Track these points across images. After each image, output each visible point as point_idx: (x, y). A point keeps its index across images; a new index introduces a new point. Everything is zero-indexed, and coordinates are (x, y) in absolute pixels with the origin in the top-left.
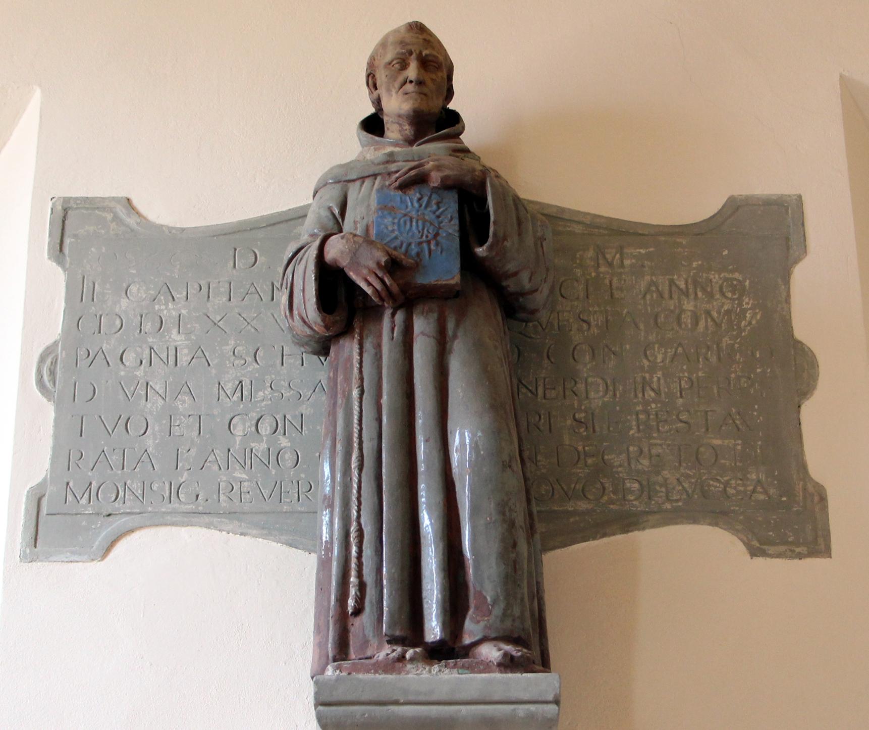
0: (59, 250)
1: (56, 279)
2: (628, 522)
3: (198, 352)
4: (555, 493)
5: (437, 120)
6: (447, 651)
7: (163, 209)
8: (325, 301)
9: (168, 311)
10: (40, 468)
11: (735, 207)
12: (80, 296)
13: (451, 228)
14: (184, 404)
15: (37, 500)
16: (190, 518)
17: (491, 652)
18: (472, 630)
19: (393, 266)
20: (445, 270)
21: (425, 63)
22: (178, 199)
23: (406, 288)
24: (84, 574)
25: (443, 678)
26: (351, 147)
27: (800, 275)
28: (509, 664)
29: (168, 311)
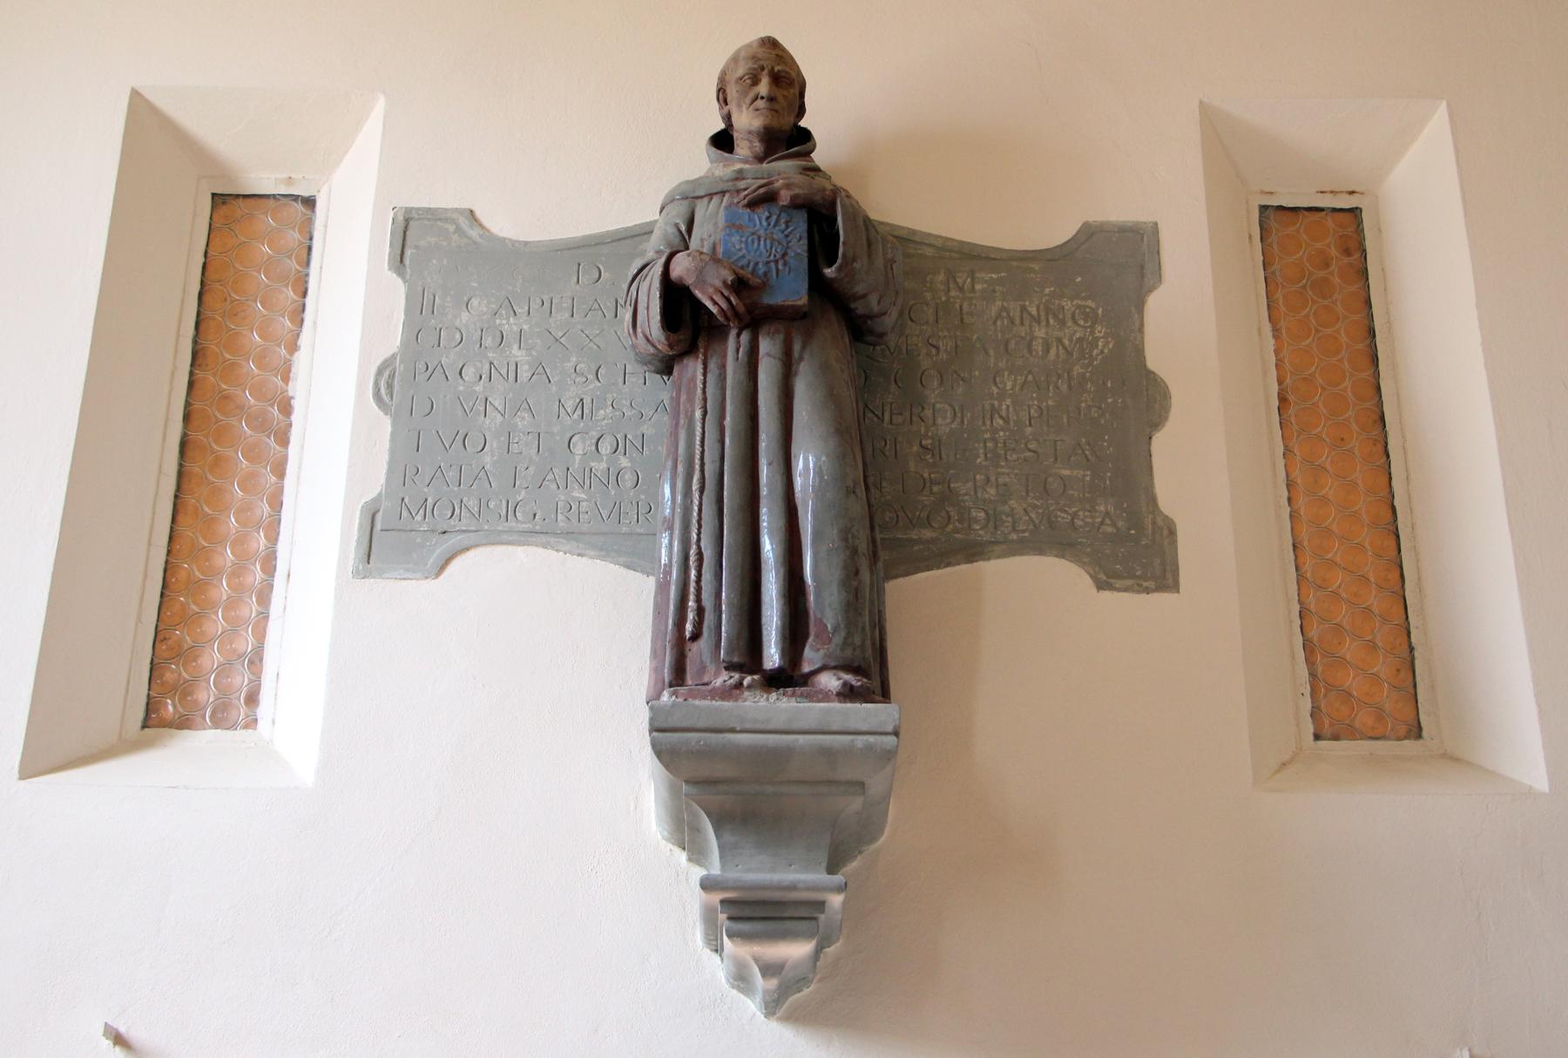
0: (399, 261)
1: (397, 290)
2: (973, 552)
4: (898, 522)
5: (788, 138)
7: (504, 223)
8: (670, 319)
9: (509, 325)
10: (376, 482)
11: (1089, 233)
12: (420, 308)
14: (523, 421)
15: (372, 515)
16: (527, 537)
17: (830, 681)
18: (811, 657)
19: (740, 285)
20: (792, 290)
21: (776, 79)
23: (752, 309)
25: (780, 706)
26: (700, 163)
27: (1155, 304)
29: (509, 325)
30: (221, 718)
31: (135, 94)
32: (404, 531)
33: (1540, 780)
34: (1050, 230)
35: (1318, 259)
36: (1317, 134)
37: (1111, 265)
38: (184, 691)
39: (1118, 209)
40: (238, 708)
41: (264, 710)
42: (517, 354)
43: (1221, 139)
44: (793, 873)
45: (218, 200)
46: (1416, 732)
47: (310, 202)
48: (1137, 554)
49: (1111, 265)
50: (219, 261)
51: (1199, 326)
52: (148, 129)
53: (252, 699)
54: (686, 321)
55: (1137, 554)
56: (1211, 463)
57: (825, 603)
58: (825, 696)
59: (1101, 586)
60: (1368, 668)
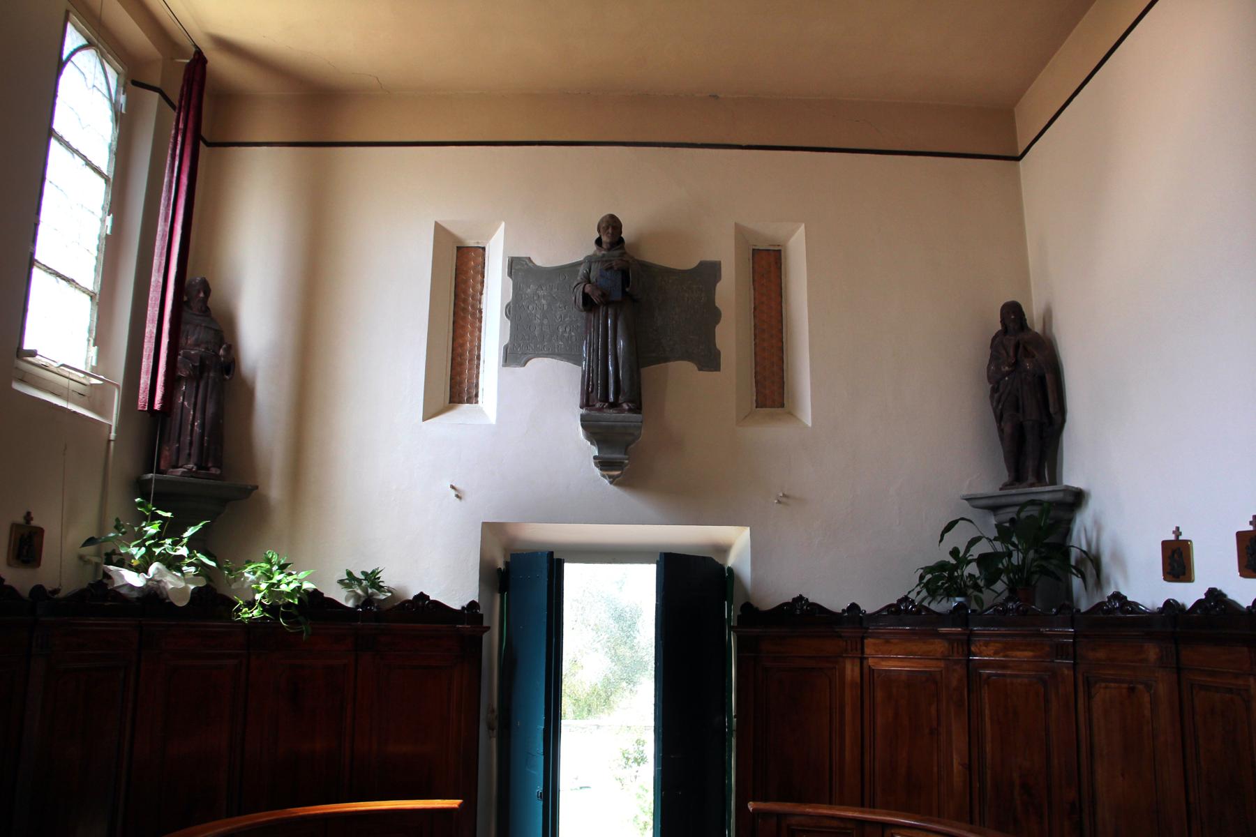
0: (510, 274)
1: (510, 282)
2: (666, 360)
3: (549, 305)
4: (647, 351)
5: (618, 242)
6: (614, 405)
7: (539, 261)
8: (585, 303)
9: (541, 293)
10: (507, 340)
11: (702, 264)
12: (517, 289)
13: (619, 283)
14: (545, 322)
15: (506, 348)
16: (546, 355)
17: (625, 406)
18: (621, 399)
19: (603, 295)
20: (617, 296)
21: (614, 228)
22: (543, 259)
23: (607, 301)
24: (519, 370)
25: (611, 414)
26: (592, 249)
27: (719, 287)
28: (630, 410)
29: (541, 293)
30: (469, 401)
31: (436, 223)
32: (514, 355)
33: (810, 425)
34: (691, 264)
35: (767, 265)
36: (767, 229)
37: (710, 272)
38: (461, 393)
39: (711, 257)
40: (473, 398)
41: (480, 399)
42: (544, 302)
43: (740, 231)
44: (617, 456)
45: (458, 248)
46: (782, 405)
47: (484, 249)
48: (709, 360)
49: (710, 272)
50: (460, 268)
51: (731, 293)
52: (439, 229)
53: (477, 395)
54: (588, 303)
55: (709, 360)
56: (732, 336)
57: (625, 385)
58: (623, 411)
59: (700, 369)
60: (771, 389)
